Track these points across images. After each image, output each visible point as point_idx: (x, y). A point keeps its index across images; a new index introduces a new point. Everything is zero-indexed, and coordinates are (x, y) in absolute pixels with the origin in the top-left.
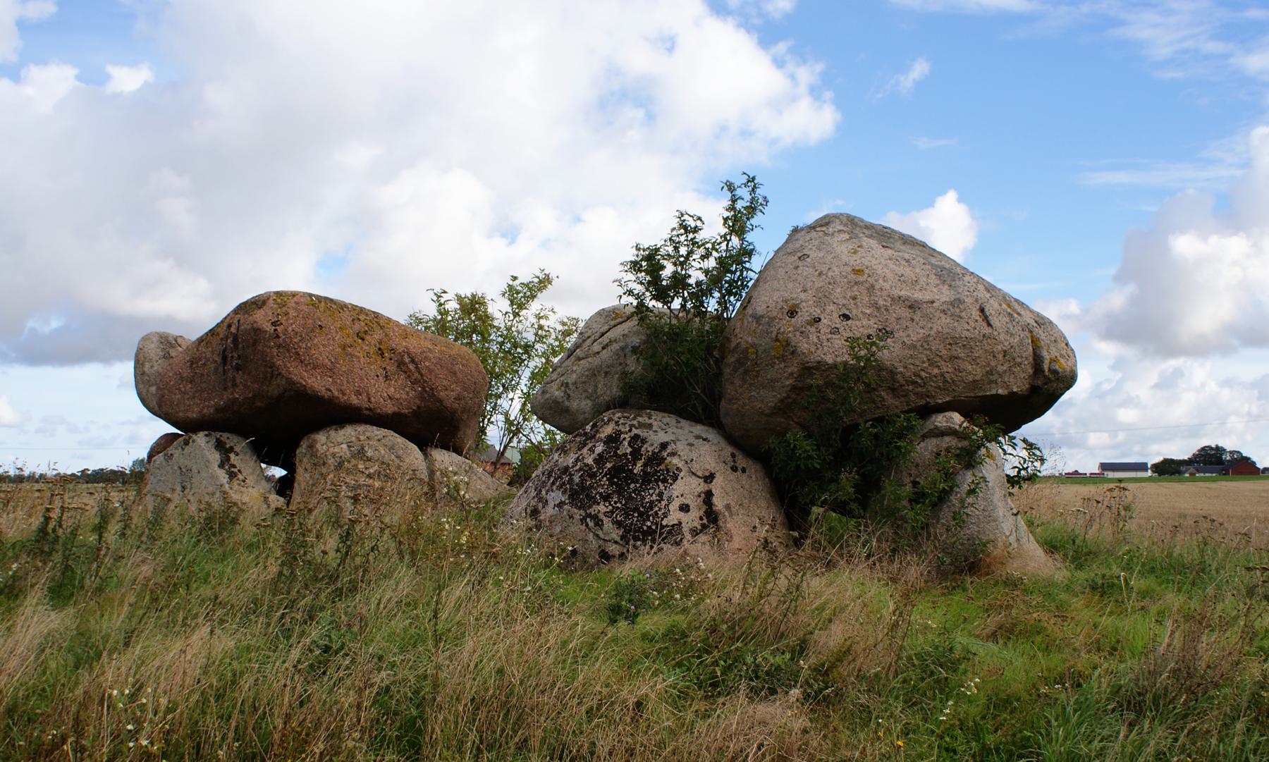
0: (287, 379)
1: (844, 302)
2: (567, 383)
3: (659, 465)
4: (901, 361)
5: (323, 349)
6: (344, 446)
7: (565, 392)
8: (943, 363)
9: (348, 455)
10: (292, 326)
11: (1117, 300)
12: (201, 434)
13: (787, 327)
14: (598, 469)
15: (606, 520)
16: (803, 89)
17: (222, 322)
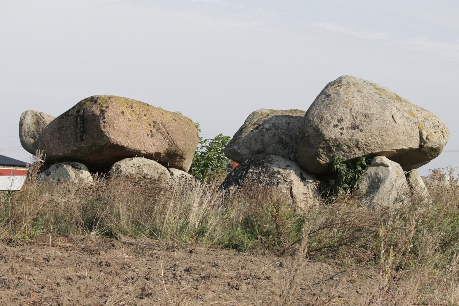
4: (360, 137)
8: (377, 137)
17: (73, 108)
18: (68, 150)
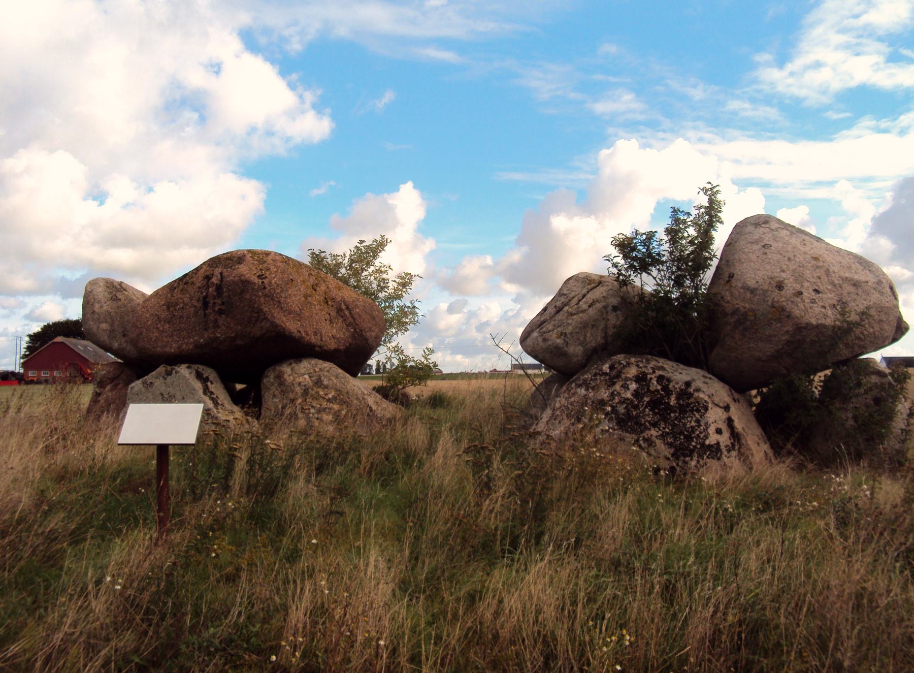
0: (272, 322)
1: (814, 280)
2: (566, 333)
3: (689, 398)
5: (294, 298)
6: (307, 376)
7: (564, 340)
9: (311, 384)
10: (274, 279)
11: (516, 256)
12: (183, 366)
13: (775, 295)
14: (639, 402)
15: (658, 442)
16: (308, 105)
17: (197, 270)
18: (187, 344)
